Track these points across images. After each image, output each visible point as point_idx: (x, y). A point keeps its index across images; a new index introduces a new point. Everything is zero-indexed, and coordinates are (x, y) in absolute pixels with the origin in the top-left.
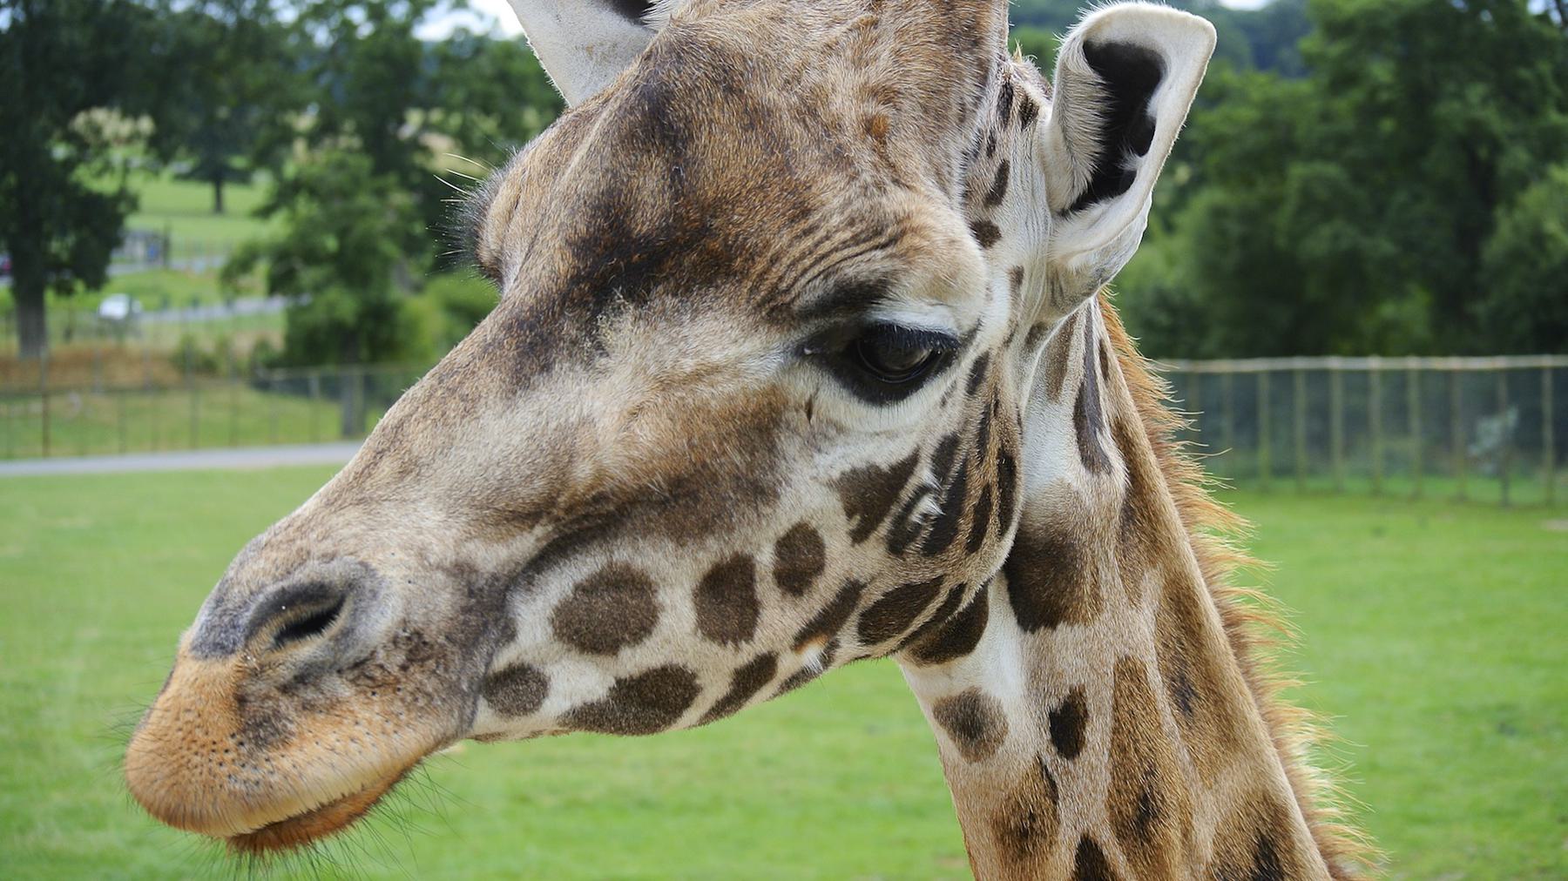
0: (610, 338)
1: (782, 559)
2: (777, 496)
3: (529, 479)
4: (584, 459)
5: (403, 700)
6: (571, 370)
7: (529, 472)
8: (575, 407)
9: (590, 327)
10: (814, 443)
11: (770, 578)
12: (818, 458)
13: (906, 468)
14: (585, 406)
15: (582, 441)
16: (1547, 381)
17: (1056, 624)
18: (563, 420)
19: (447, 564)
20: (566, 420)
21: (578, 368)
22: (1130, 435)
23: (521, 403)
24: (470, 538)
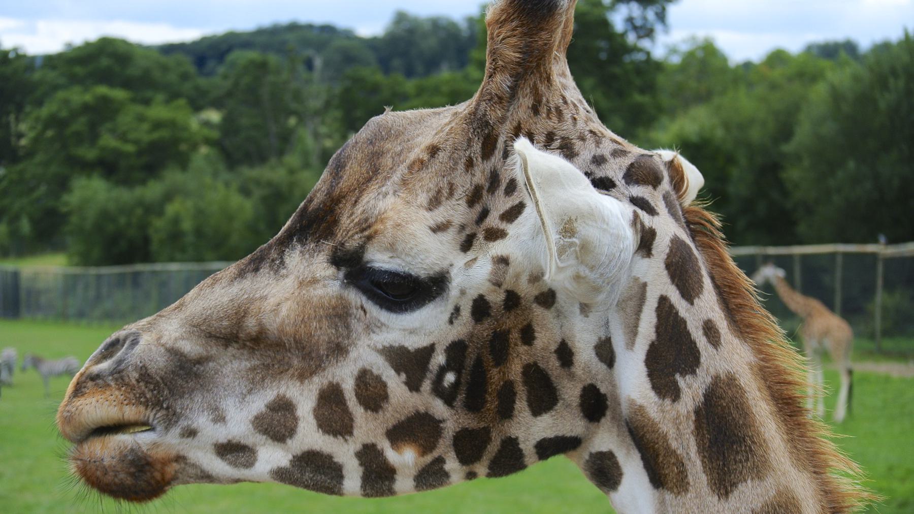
0: (287, 260)
1: (359, 388)
2: (347, 352)
3: (221, 319)
4: (252, 316)
5: (135, 395)
6: (269, 273)
7: (222, 316)
8: (261, 290)
9: (282, 254)
10: (370, 328)
11: (354, 399)
12: (372, 335)
13: (430, 350)
14: (266, 291)
15: (254, 308)
16: (839, 260)
17: (285, 440)
18: (251, 295)
19: (168, 346)
20: (253, 296)
21: (271, 272)
22: (742, 384)
23: (236, 284)
24: (183, 339)
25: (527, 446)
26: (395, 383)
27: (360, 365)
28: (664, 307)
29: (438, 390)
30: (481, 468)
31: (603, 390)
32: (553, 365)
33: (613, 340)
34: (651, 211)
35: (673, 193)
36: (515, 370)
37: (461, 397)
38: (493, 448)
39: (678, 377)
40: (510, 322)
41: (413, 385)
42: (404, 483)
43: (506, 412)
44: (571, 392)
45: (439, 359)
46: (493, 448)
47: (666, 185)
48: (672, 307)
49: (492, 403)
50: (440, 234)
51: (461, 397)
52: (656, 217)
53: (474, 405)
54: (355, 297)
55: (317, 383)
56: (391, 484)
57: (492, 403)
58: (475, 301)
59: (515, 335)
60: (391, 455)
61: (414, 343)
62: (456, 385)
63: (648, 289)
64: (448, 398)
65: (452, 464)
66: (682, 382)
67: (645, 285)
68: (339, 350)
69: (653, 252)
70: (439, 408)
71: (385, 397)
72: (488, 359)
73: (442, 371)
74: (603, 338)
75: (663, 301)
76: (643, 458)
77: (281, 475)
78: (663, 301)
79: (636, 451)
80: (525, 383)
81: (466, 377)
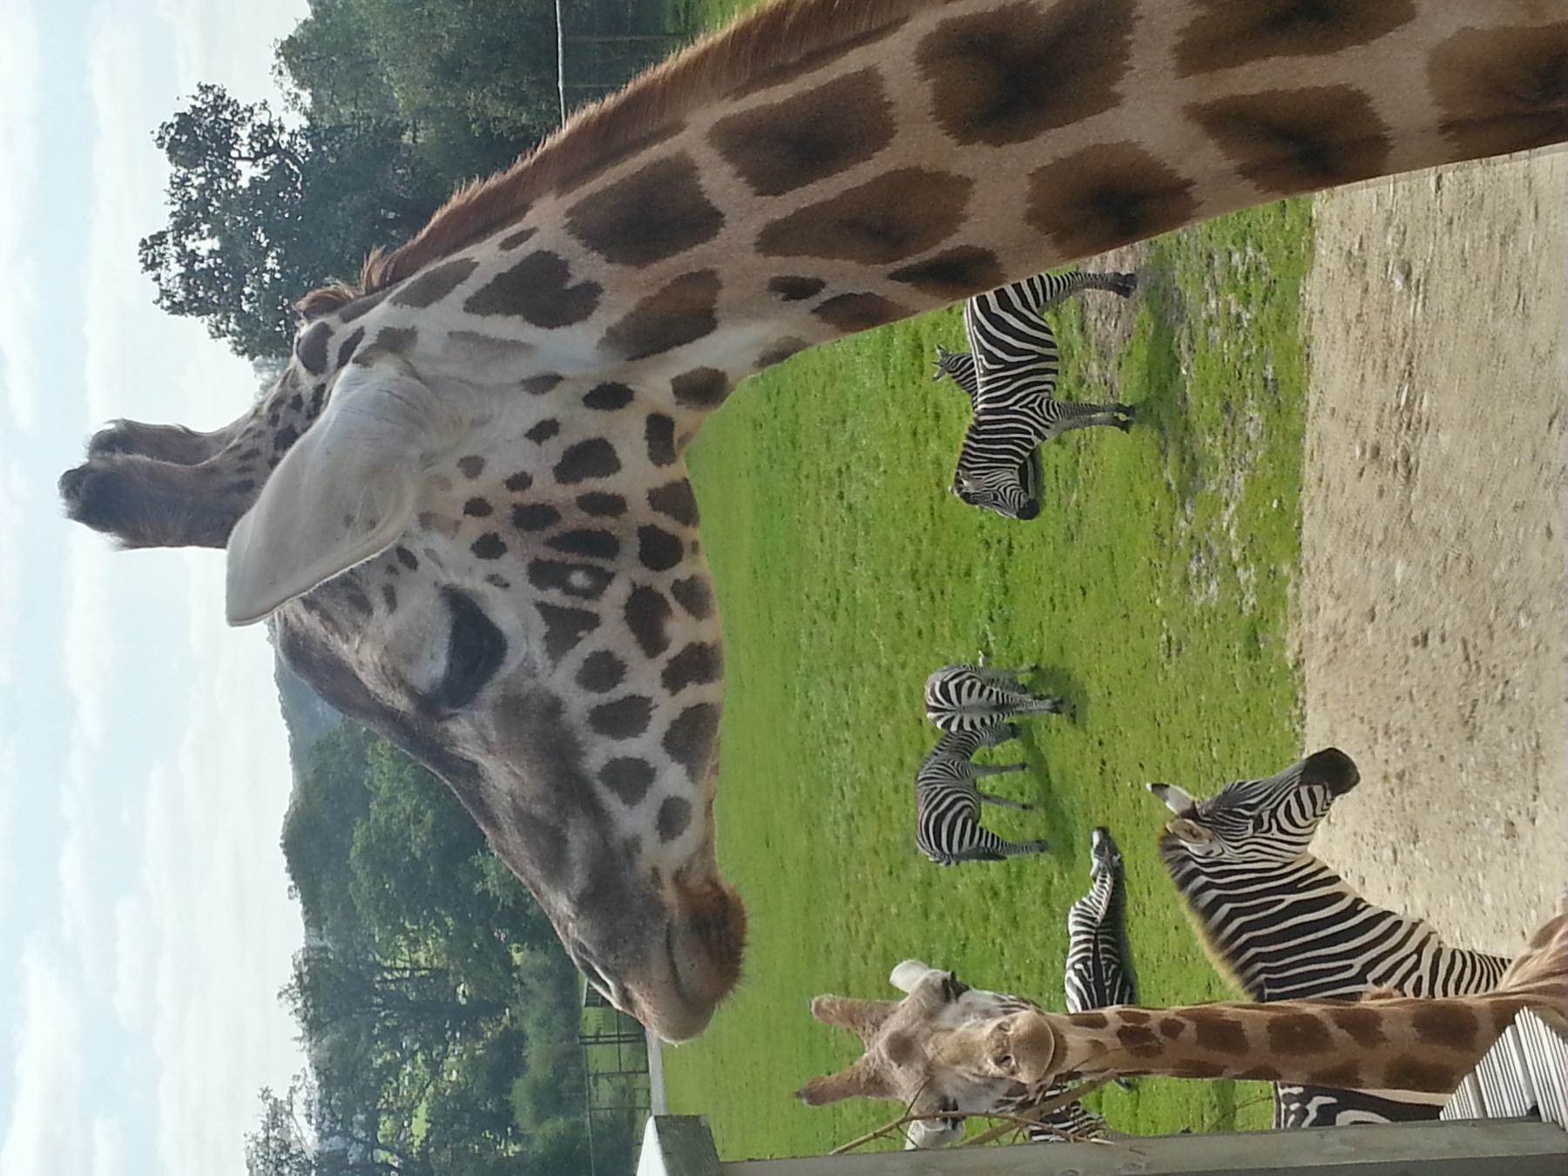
10: (531, 673)
13: (545, 609)
25: (661, 476)
26: (591, 643)
27: (572, 685)
28: (478, 305)
29: (591, 594)
30: (688, 534)
31: (593, 387)
32: (554, 449)
33: (525, 377)
34: (359, 334)
35: (342, 310)
36: (563, 495)
37: (599, 562)
38: (665, 523)
39: (570, 284)
40: (503, 502)
41: (592, 621)
42: (705, 632)
43: (613, 505)
44: (592, 424)
45: (554, 596)
46: (665, 523)
47: (331, 320)
48: (478, 295)
49: (606, 523)
50: (399, 598)
51: (599, 562)
52: (366, 330)
53: (606, 545)
54: (490, 693)
55: (585, 734)
56: (1171, 1070)
57: (606, 523)
58: (480, 556)
59: (518, 497)
60: (675, 648)
61: (540, 627)
62: (590, 570)
63: (456, 329)
64: (603, 579)
65: (681, 571)
66: (577, 277)
67: (451, 334)
68: (554, 707)
69: (409, 326)
70: (618, 592)
71: (607, 655)
72: (553, 531)
73: (569, 590)
74: (522, 387)
75: (473, 306)
76: (679, 344)
77: (693, 774)
78: (473, 306)
79: (670, 353)
80: (577, 480)
81: (572, 558)
